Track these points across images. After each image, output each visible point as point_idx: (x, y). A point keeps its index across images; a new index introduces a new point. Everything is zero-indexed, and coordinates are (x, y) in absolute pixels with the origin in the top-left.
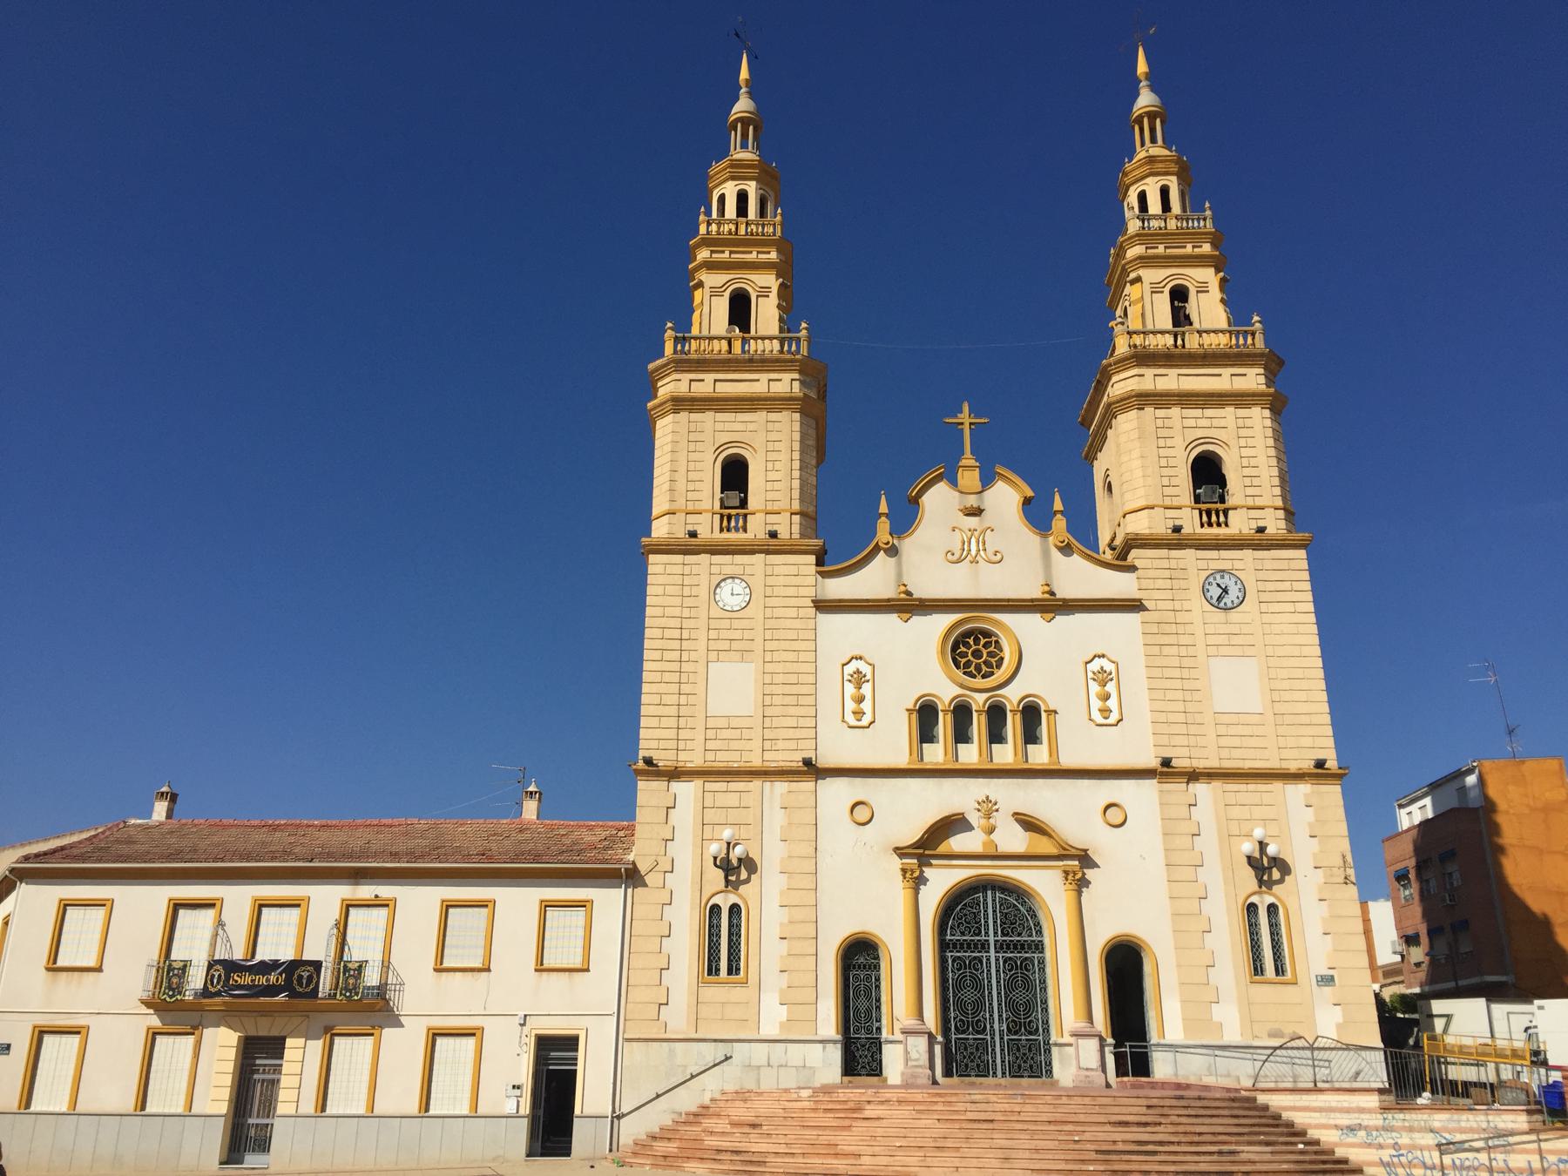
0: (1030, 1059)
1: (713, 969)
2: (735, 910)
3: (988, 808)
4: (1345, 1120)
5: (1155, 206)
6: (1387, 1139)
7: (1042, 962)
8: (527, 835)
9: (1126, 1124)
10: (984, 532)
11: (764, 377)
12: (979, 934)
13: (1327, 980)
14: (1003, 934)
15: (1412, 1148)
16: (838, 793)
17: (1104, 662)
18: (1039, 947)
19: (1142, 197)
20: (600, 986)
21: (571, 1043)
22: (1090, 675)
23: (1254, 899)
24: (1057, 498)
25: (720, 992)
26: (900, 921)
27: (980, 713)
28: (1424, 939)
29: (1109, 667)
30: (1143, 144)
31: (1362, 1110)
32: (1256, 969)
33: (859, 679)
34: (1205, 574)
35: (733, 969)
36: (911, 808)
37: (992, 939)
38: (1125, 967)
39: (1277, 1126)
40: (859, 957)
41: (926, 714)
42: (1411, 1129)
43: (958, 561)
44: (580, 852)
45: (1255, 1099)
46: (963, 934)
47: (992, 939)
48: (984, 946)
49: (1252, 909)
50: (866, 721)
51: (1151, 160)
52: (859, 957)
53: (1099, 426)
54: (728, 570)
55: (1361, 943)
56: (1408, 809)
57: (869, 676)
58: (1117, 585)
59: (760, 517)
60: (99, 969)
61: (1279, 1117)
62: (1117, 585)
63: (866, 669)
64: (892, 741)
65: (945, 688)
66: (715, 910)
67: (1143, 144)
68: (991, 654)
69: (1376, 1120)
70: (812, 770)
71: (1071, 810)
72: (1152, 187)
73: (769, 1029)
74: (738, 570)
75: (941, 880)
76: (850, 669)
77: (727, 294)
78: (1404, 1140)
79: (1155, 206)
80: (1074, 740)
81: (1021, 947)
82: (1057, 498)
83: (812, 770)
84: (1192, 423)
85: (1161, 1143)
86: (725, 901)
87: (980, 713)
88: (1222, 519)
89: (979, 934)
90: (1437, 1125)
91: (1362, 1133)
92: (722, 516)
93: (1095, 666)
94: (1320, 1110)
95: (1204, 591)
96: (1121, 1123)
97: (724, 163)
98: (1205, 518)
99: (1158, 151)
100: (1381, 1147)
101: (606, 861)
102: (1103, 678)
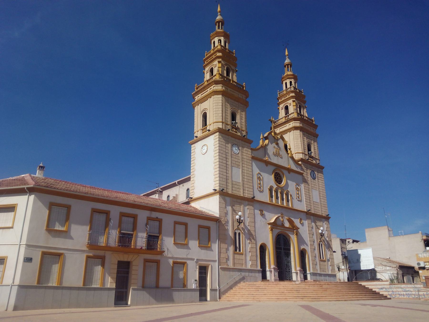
0: (290, 279)
4: (380, 287)
5: (288, 86)
6: (391, 290)
11: (209, 89)
15: (396, 291)
19: (286, 83)
26: (269, 240)
40: (263, 248)
42: (396, 288)
51: (287, 75)
55: (75, 292)
60: (12, 228)
69: (388, 287)
72: (288, 81)
73: (249, 267)
78: (395, 290)
79: (288, 86)
90: (402, 287)
91: (384, 289)
94: (373, 285)
97: (214, 33)
99: (289, 73)
100: (389, 292)
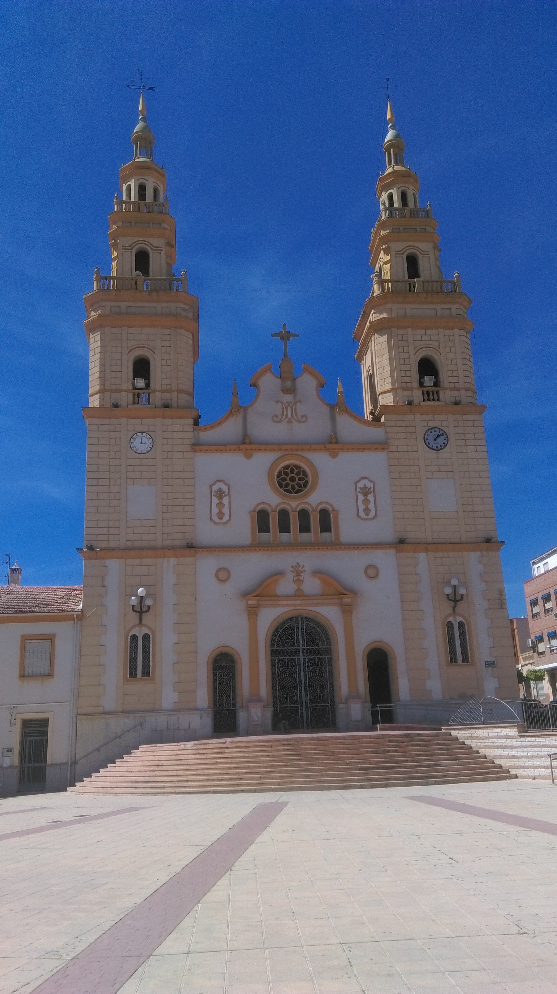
1: (133, 674)
2: (146, 638)
3: (298, 571)
7: (330, 660)
8: (12, 596)
9: (377, 752)
10: (295, 403)
12: (294, 645)
13: (491, 664)
14: (308, 645)
16: (207, 565)
17: (365, 482)
18: (329, 651)
20: (61, 685)
21: (44, 723)
22: (359, 490)
23: (451, 619)
24: (339, 385)
25: (139, 687)
27: (294, 517)
28: (554, 598)
29: (369, 485)
30: (390, 163)
31: (508, 737)
32: (451, 659)
33: (220, 494)
34: (426, 429)
35: (146, 673)
36: (252, 567)
37: (301, 648)
38: (379, 663)
39: (462, 748)
41: (262, 520)
43: (278, 422)
44: (48, 605)
45: (450, 735)
46: (284, 646)
47: (301, 648)
48: (297, 652)
49: (450, 625)
50: (226, 518)
52: (224, 667)
53: (365, 339)
54: (139, 428)
56: (537, 565)
57: (227, 493)
58: (376, 433)
59: (158, 395)
61: (464, 743)
62: (376, 433)
63: (225, 488)
64: (242, 529)
65: (273, 500)
66: (134, 638)
67: (390, 163)
68: (298, 474)
70: (191, 547)
71: (347, 566)
74: (145, 428)
75: (269, 617)
76: (215, 488)
77: (134, 252)
80: (348, 528)
81: (319, 652)
82: (339, 385)
83: (191, 547)
84: (418, 338)
85: (396, 762)
86: (139, 632)
87: (294, 517)
88: (436, 397)
89: (294, 645)
92: (134, 394)
93: (360, 485)
95: (425, 440)
96: (374, 752)
98: (426, 397)
101: (64, 611)
102: (365, 492)
